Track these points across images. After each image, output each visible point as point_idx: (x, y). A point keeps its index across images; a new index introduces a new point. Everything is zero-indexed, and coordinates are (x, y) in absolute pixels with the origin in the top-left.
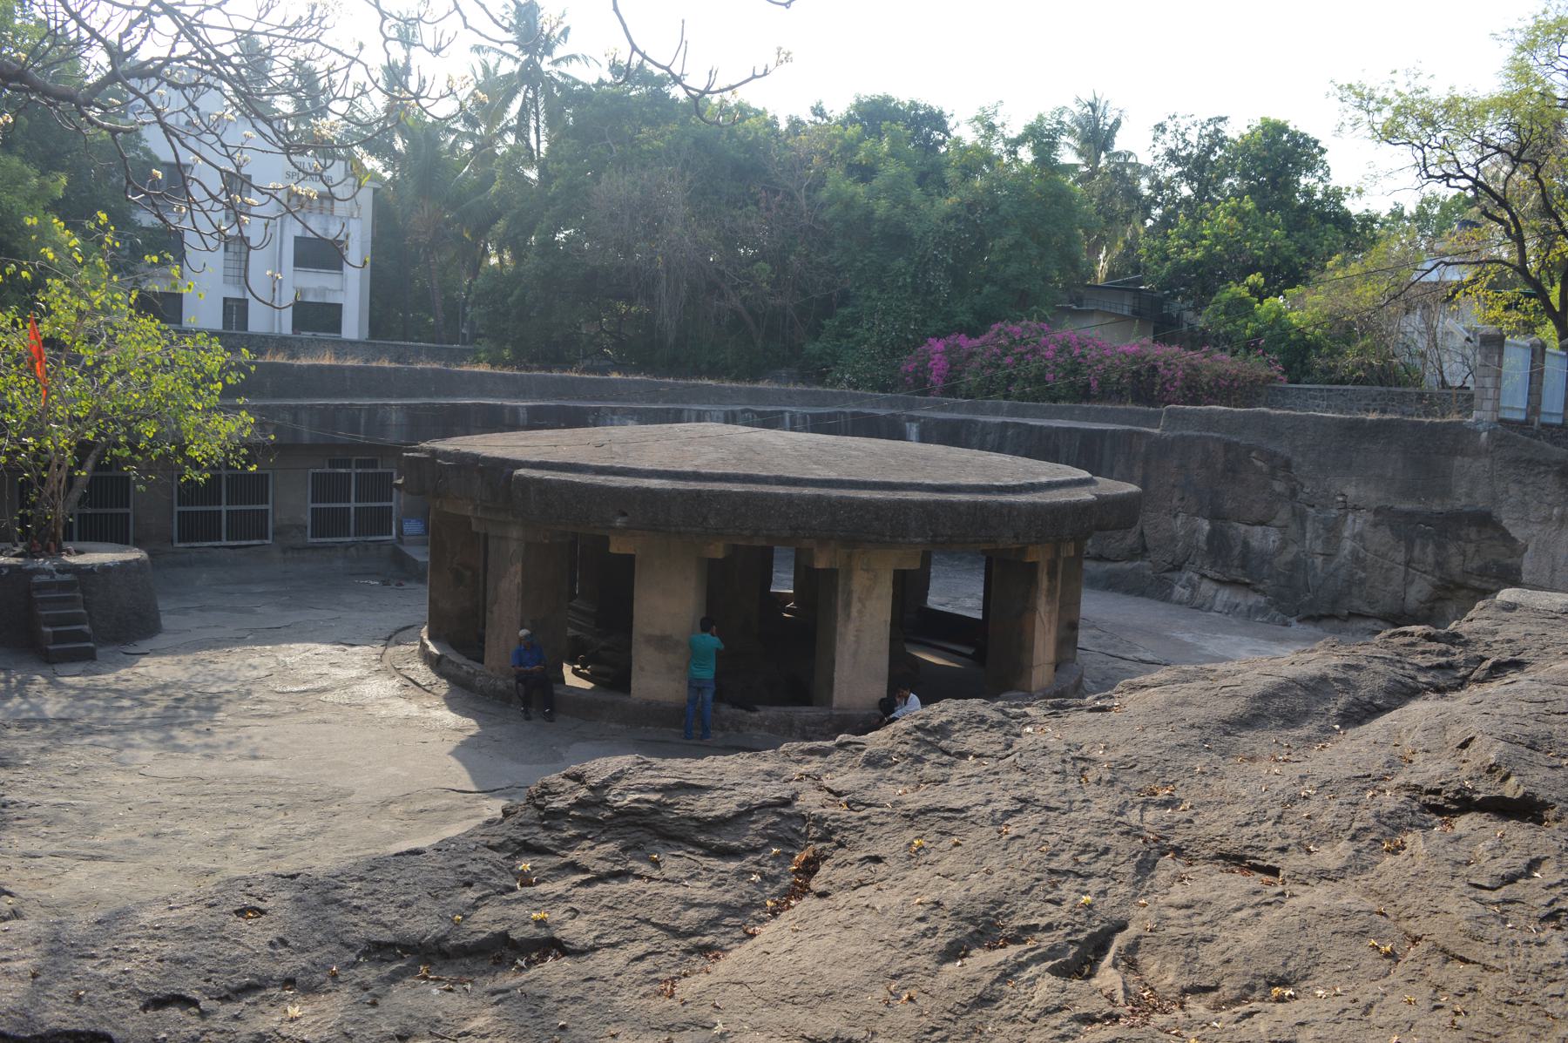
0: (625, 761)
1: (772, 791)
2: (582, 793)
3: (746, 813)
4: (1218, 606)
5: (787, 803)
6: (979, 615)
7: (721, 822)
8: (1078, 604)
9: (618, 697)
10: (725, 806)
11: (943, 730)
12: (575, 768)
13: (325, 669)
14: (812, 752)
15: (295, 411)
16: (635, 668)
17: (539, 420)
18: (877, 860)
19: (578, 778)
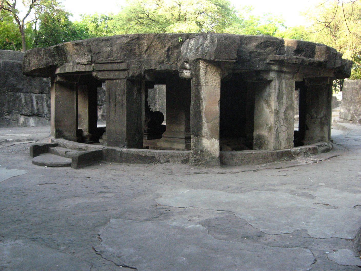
9: (263, 151)
17: (32, 106)
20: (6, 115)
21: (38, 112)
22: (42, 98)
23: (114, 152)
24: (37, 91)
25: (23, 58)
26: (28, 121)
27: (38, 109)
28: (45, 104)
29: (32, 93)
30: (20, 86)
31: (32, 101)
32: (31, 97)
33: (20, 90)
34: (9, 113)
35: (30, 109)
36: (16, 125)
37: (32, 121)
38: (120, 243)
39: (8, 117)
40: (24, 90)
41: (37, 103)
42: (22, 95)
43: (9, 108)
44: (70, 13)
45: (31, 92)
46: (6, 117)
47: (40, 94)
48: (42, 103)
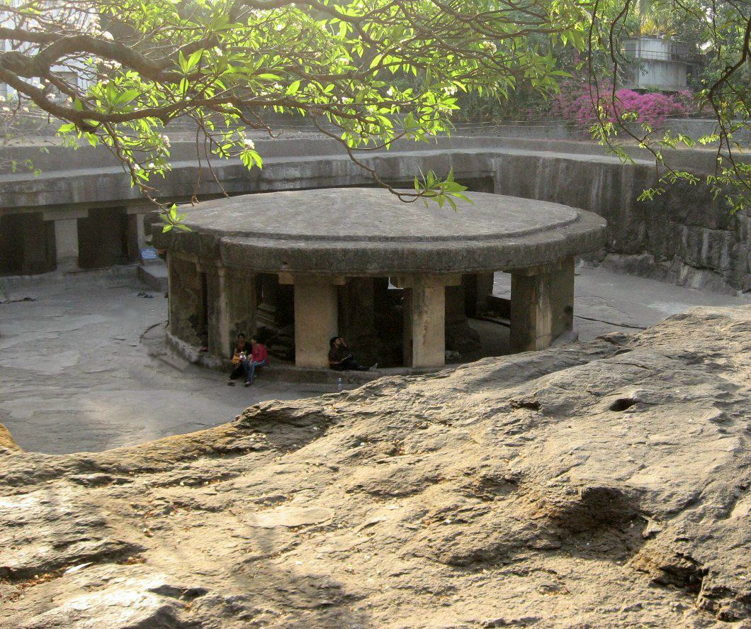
0: (271, 402)
1: (316, 409)
2: (259, 411)
3: (307, 415)
4: (14, 168)
5: (319, 412)
6: (508, 297)
7: (300, 418)
8: (141, 256)
9: (291, 368)
10: (300, 414)
11: (378, 388)
12: (257, 405)
13: (110, 357)
14: (332, 396)
15: (612, 150)
16: (297, 349)
17: (700, 250)
18: (343, 426)
19: (258, 407)
20: (664, 261)
21: (709, 263)
22: (721, 239)
23: (338, 342)
24: (714, 224)
25: (381, 225)
26: (691, 278)
27: (709, 258)
28: (725, 251)
29: (705, 227)
30: (683, 214)
31: (700, 243)
32: (700, 235)
33: (682, 220)
34: (670, 258)
35: (695, 255)
36: (675, 280)
37: (698, 277)
38: (467, 474)
39: (668, 264)
40: (689, 221)
41: (710, 247)
42: (685, 230)
43: (667, 248)
44: (81, 276)
45: (701, 225)
46: (663, 263)
47: (719, 231)
48: (720, 248)
